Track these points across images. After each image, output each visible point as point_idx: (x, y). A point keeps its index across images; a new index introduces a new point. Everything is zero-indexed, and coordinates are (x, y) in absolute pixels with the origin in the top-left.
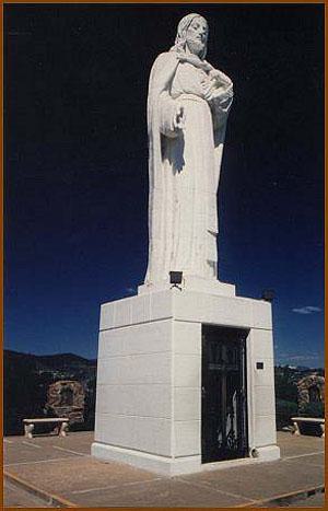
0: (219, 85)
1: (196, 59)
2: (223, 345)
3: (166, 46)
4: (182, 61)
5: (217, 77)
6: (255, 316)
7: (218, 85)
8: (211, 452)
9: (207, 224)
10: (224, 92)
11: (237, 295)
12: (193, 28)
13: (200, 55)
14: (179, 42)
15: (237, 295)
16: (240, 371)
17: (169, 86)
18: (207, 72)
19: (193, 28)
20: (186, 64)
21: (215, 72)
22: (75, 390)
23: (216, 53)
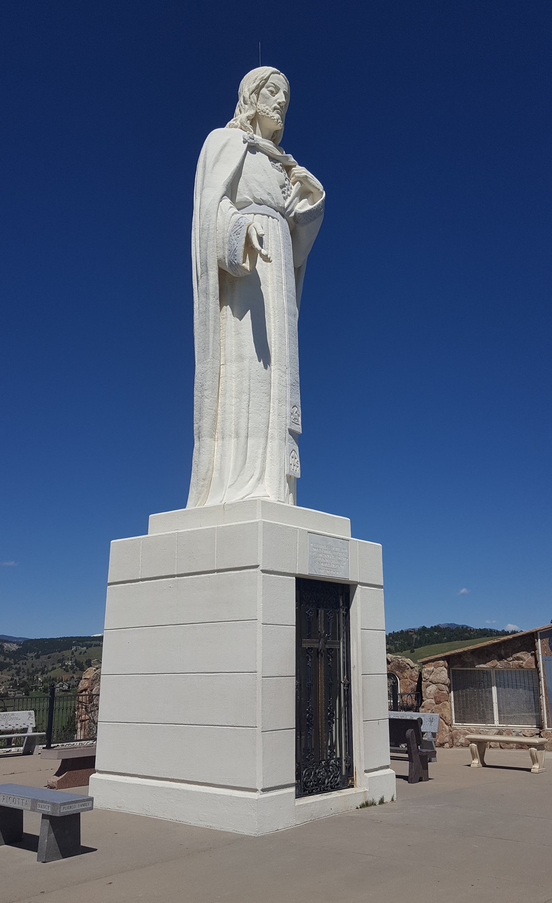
0: (304, 194)
1: (267, 144)
2: (322, 603)
3: (223, 117)
4: (253, 148)
5: (303, 180)
6: (359, 560)
7: (303, 191)
8: (306, 786)
9: (288, 421)
10: (309, 207)
11: (21, 811)
12: (264, 89)
13: (273, 137)
14: (242, 114)
15: (21, 811)
16: (332, 653)
17: (231, 191)
18: (288, 169)
19: (264, 89)
20: (259, 154)
21: (300, 171)
22: (252, 112)
23: (297, 138)
